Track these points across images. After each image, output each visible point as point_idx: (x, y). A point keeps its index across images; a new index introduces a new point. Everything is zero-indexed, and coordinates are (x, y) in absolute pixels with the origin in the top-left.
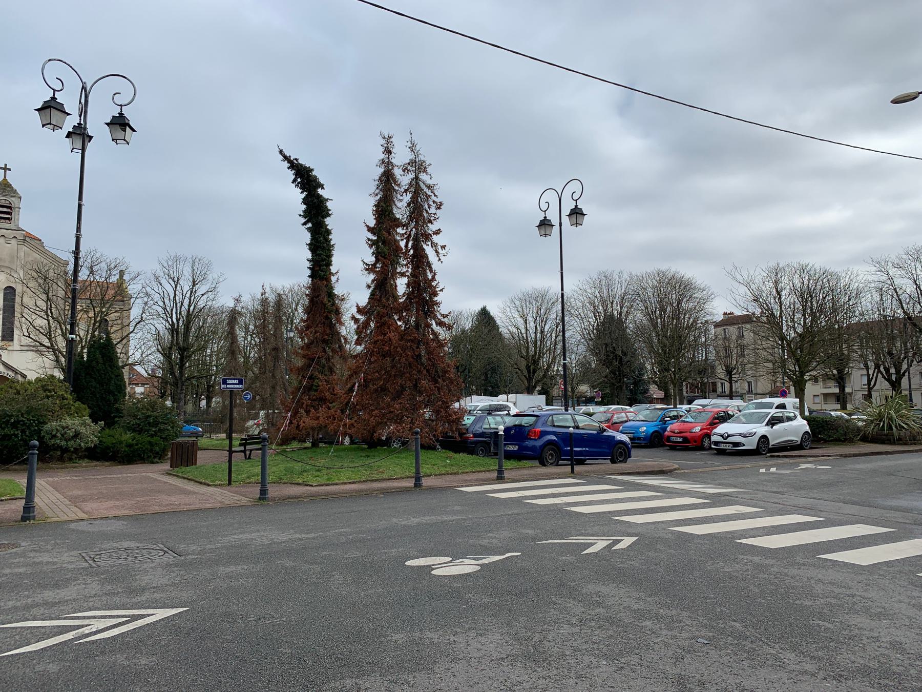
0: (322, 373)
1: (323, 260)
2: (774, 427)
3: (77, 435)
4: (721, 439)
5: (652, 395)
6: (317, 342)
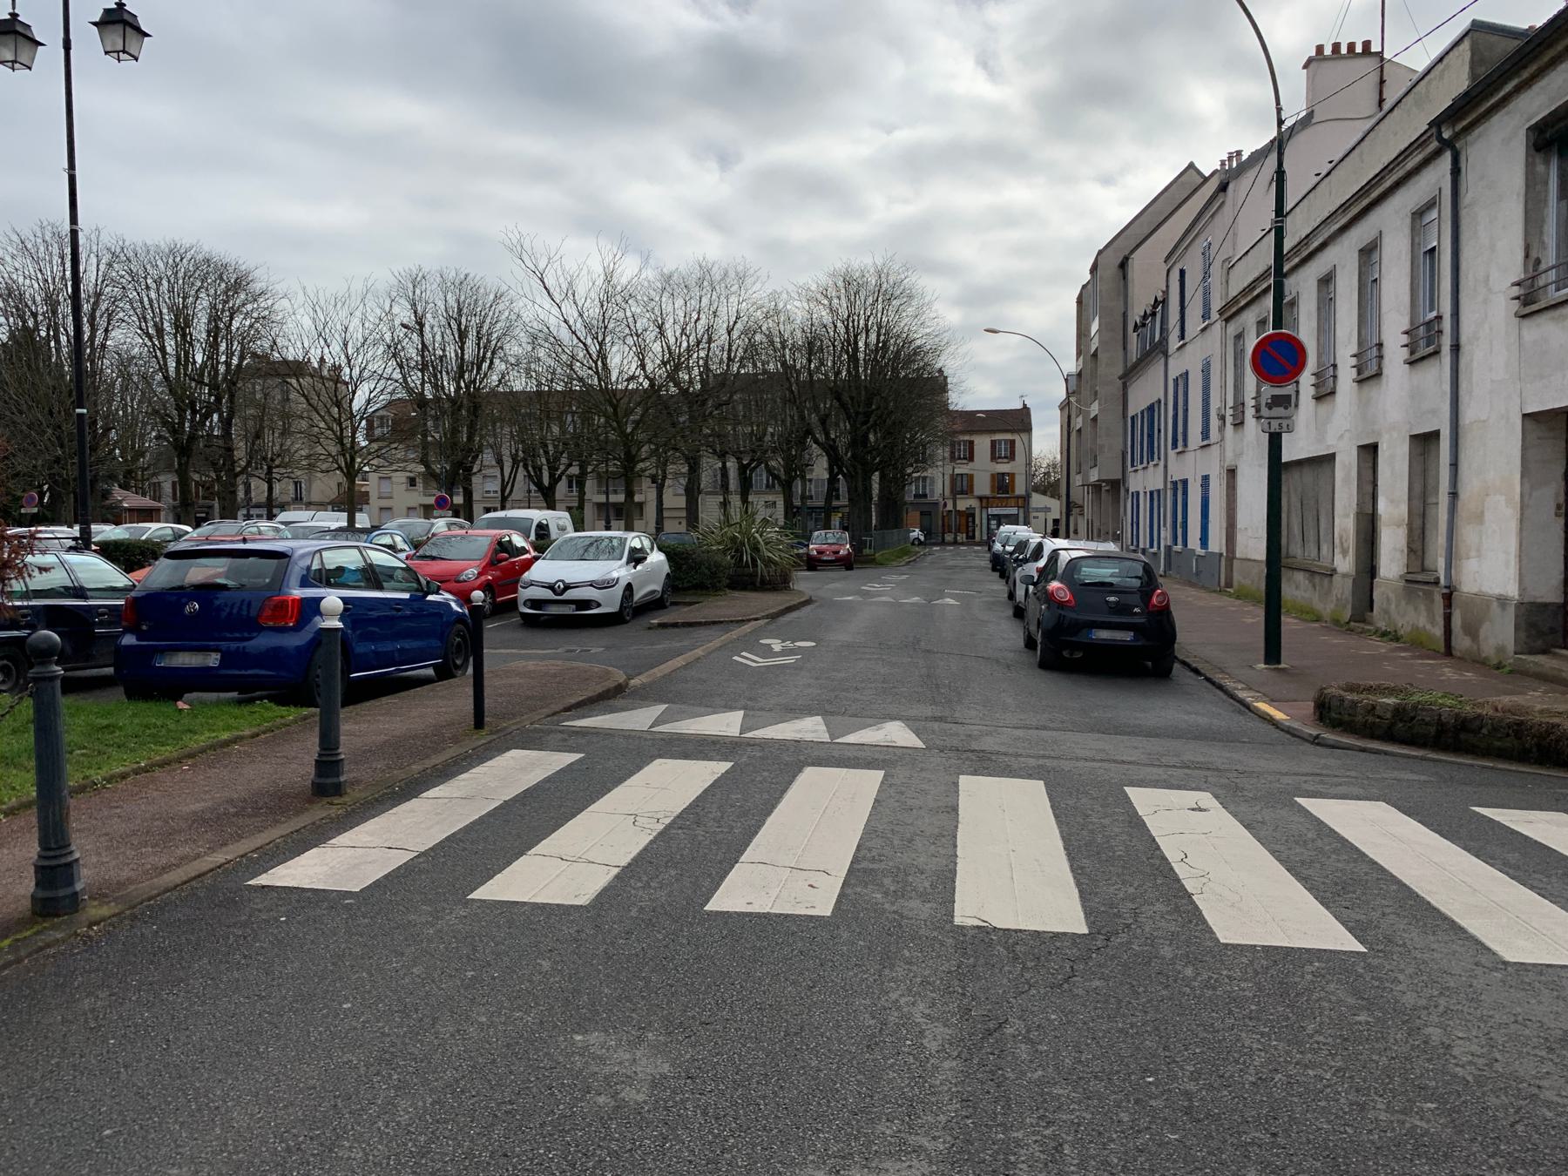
2: (639, 567)
4: (549, 594)
5: (121, 501)
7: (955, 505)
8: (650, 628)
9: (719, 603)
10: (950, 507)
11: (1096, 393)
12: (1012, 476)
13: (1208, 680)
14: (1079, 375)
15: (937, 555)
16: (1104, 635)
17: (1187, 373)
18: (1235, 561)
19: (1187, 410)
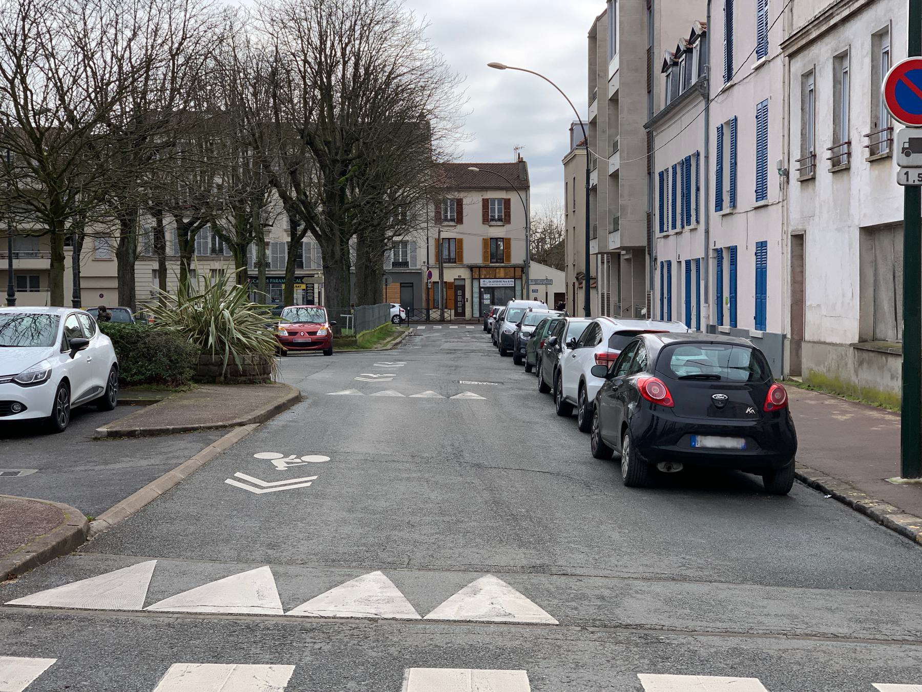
2: (78, 355)
7: (441, 275)
8: (96, 439)
9: (185, 402)
10: (435, 277)
11: (615, 145)
12: (507, 242)
13: (835, 497)
14: (593, 123)
15: (425, 335)
16: (710, 442)
17: (736, 119)
18: (803, 344)
19: (736, 164)
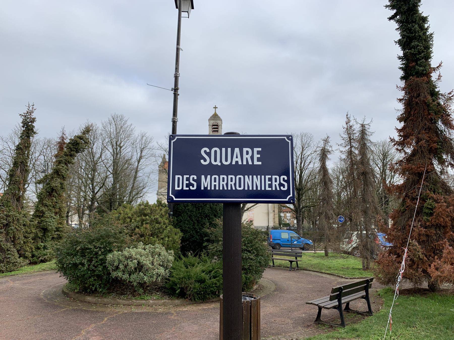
0: (434, 192)
1: (420, 53)
3: (140, 267)
6: (422, 151)
